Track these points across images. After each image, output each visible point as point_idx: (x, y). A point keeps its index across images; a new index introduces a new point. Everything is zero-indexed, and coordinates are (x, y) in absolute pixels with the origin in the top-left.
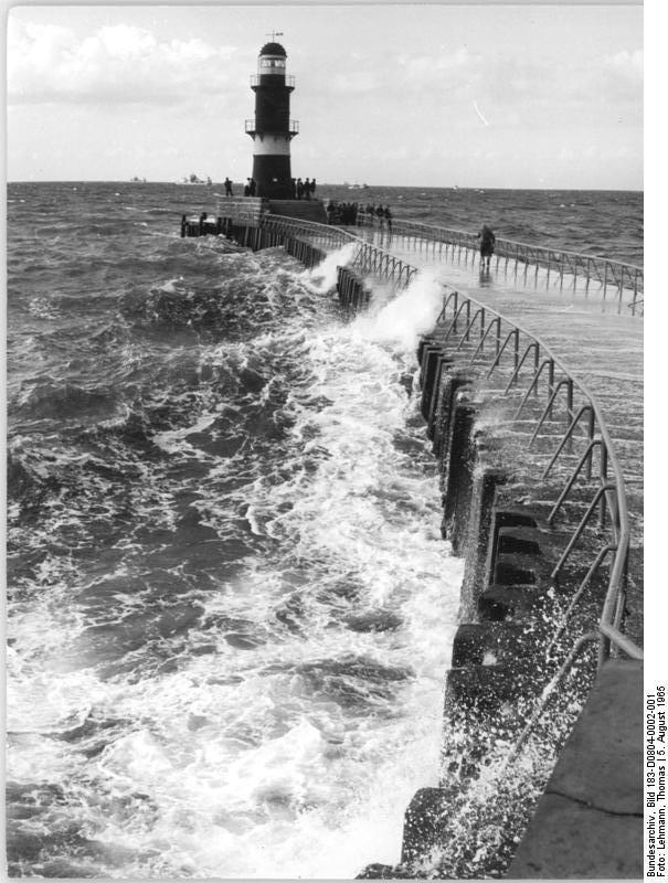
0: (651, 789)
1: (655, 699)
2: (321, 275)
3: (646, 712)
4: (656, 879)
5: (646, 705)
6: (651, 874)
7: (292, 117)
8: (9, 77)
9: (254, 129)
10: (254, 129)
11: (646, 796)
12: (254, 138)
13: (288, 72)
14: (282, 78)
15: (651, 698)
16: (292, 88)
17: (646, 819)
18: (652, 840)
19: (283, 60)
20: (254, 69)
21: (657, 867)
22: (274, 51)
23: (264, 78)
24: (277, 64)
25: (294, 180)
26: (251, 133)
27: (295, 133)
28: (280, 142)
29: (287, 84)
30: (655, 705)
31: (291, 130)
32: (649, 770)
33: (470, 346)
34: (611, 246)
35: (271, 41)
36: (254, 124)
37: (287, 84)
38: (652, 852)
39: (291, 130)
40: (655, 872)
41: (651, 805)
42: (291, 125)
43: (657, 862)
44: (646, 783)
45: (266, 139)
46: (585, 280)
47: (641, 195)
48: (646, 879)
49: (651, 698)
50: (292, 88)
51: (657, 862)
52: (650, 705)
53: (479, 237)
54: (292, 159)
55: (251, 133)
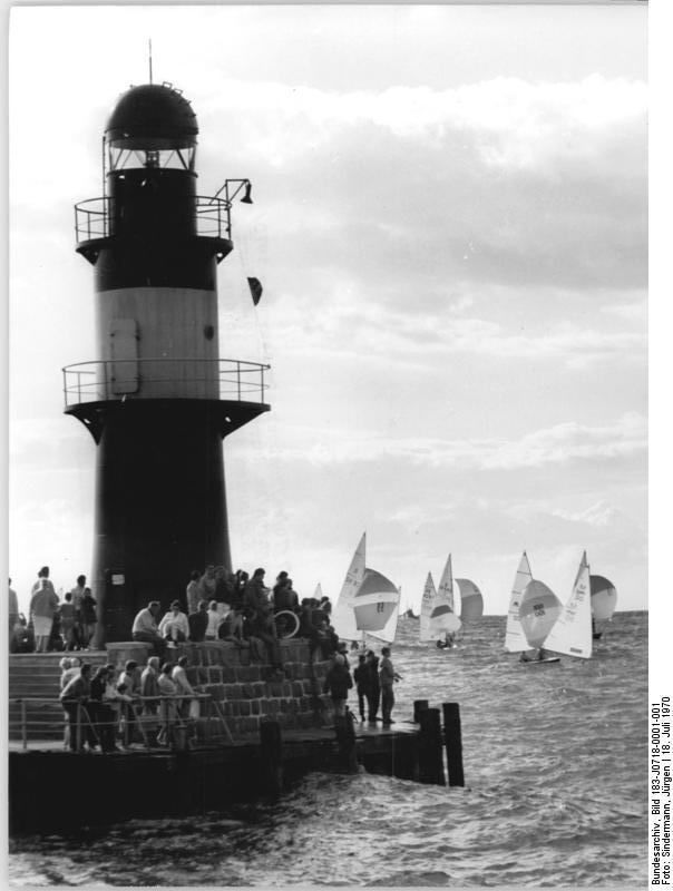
0: (656, 797)
1: (660, 707)
2: (277, 574)
3: (651, 721)
4: (661, 887)
5: (650, 714)
6: (655, 882)
8: (13, 449)
11: (651, 803)
15: (656, 727)
17: (651, 827)
18: (657, 847)
21: (662, 875)
30: (660, 733)
32: (654, 721)
34: (560, 678)
37: (206, 226)
38: (657, 860)
40: (660, 879)
41: (656, 812)
43: (662, 870)
44: (650, 790)
47: (644, 615)
48: (651, 887)
49: (656, 727)
51: (662, 870)
52: (656, 713)
53: (285, 809)
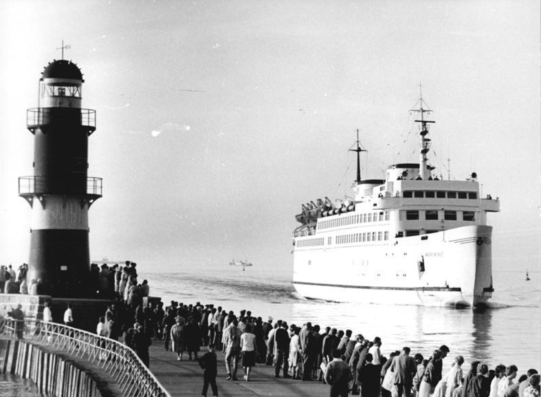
7: (91, 172)
9: (32, 191)
10: (32, 191)
12: (31, 203)
13: (84, 105)
14: (77, 113)
16: (93, 129)
19: (78, 85)
20: (39, 96)
22: (64, 73)
23: (52, 114)
24: (68, 91)
25: (109, 273)
26: (26, 196)
27: (96, 197)
28: (73, 206)
29: (85, 123)
31: (90, 191)
33: (92, 357)
35: (59, 58)
36: (32, 182)
37: (85, 123)
39: (90, 191)
42: (90, 184)
45: (49, 207)
46: (498, 394)
50: (93, 129)
54: (91, 236)
55: (26, 196)
